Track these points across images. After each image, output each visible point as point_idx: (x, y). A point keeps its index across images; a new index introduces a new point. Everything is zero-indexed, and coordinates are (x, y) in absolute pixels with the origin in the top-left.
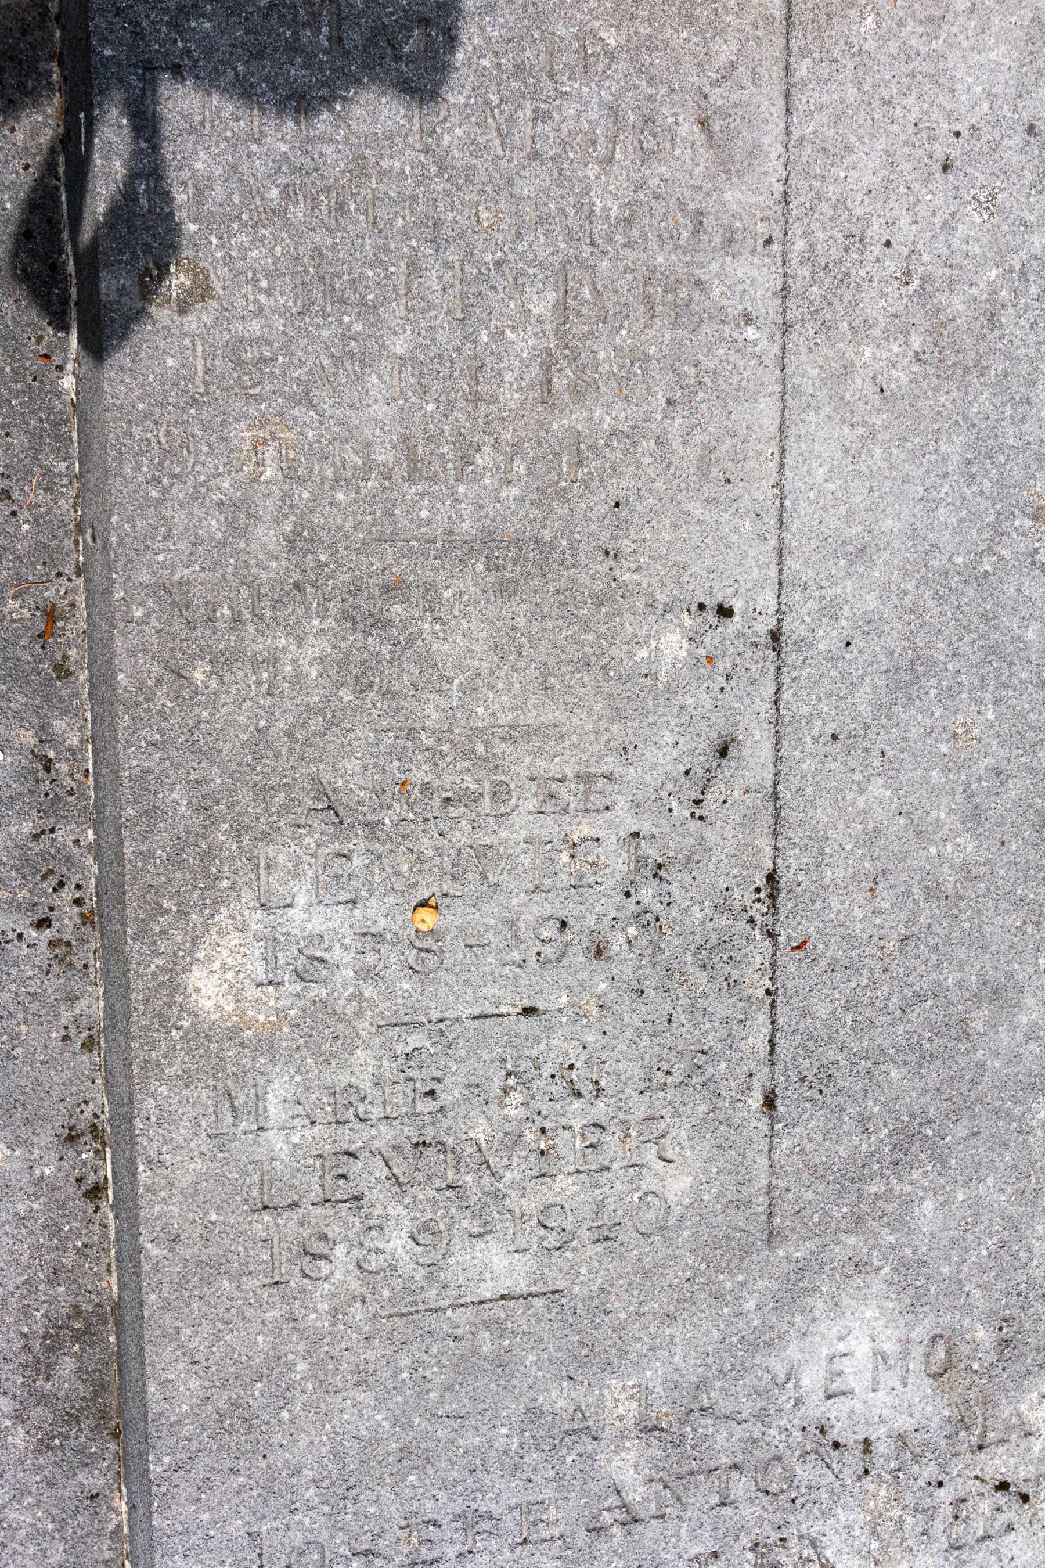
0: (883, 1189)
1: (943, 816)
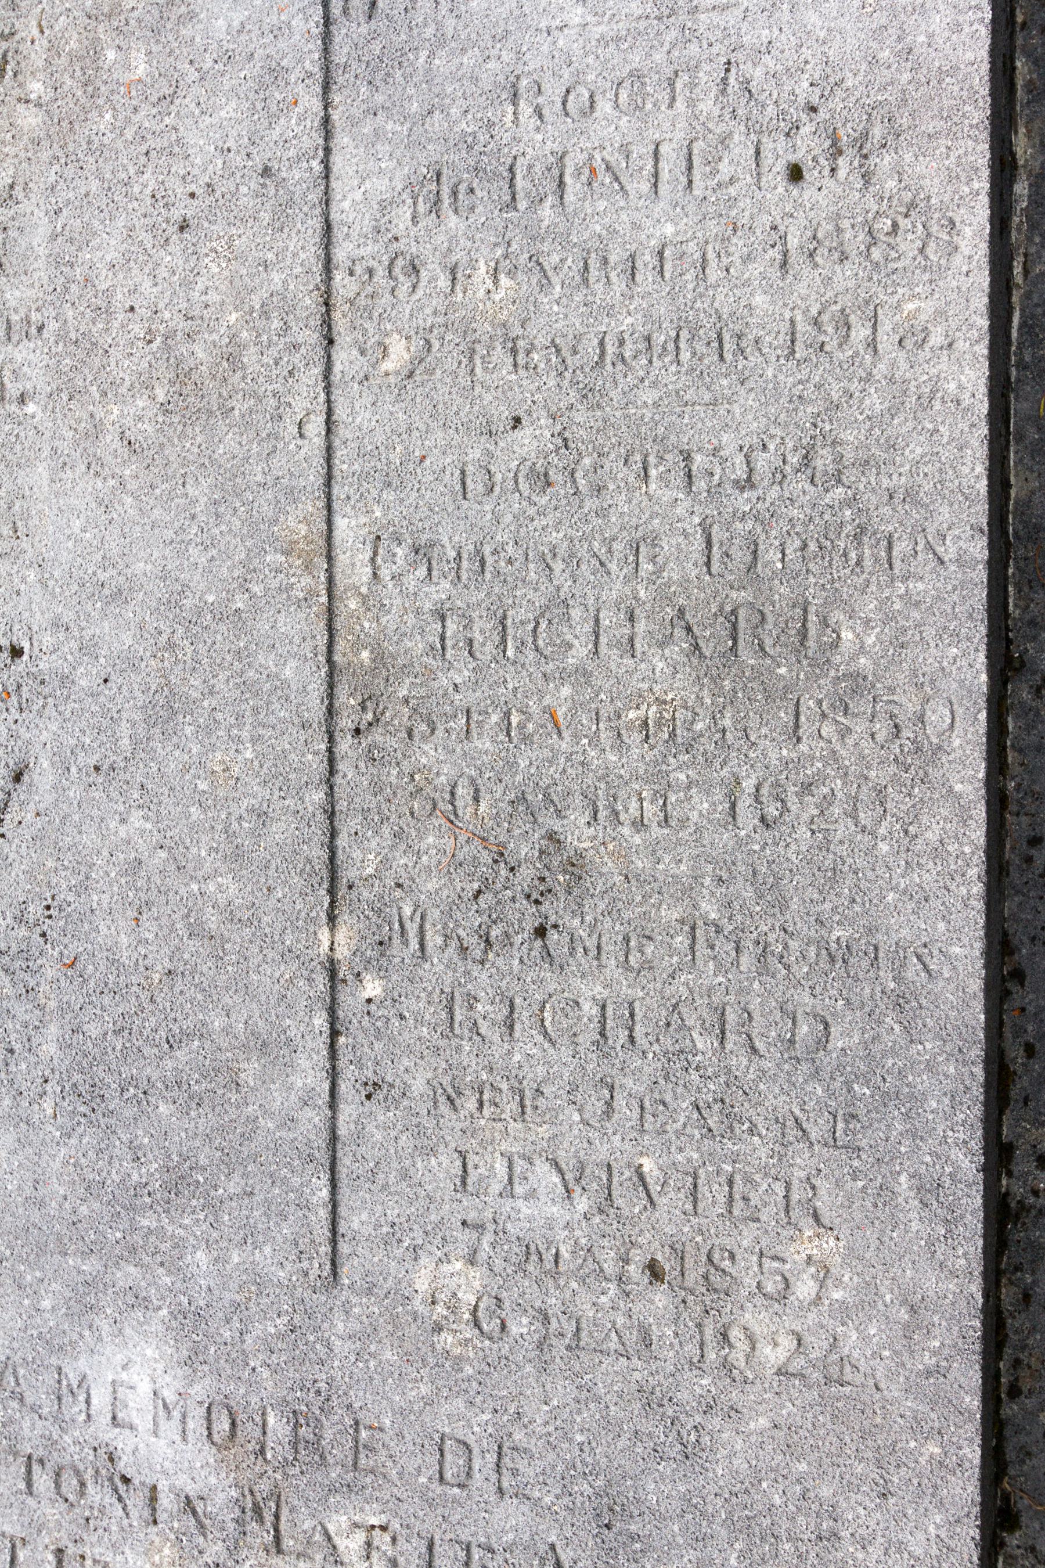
0: (155, 1224)
1: (203, 854)
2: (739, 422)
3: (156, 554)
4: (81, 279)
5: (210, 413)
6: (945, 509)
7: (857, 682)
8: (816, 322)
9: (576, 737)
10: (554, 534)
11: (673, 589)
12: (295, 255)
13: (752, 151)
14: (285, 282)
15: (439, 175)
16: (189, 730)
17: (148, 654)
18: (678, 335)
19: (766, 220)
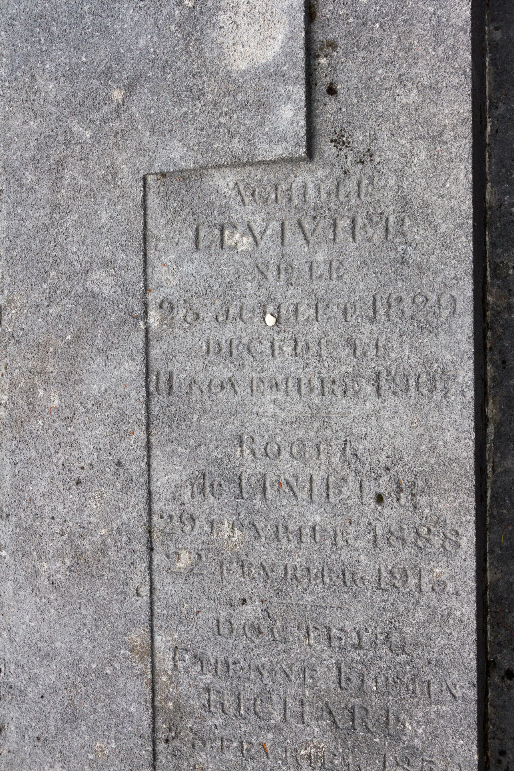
2: (354, 616)
3: (66, 640)
4: (28, 499)
5: (92, 575)
6: (456, 673)
7: (414, 751)
8: (391, 573)
9: (276, 759)
10: (263, 659)
11: (322, 693)
12: (134, 507)
13: (358, 486)
14: (129, 519)
15: (204, 475)
16: (84, 728)
17: (63, 687)
18: (323, 569)
19: (366, 520)
